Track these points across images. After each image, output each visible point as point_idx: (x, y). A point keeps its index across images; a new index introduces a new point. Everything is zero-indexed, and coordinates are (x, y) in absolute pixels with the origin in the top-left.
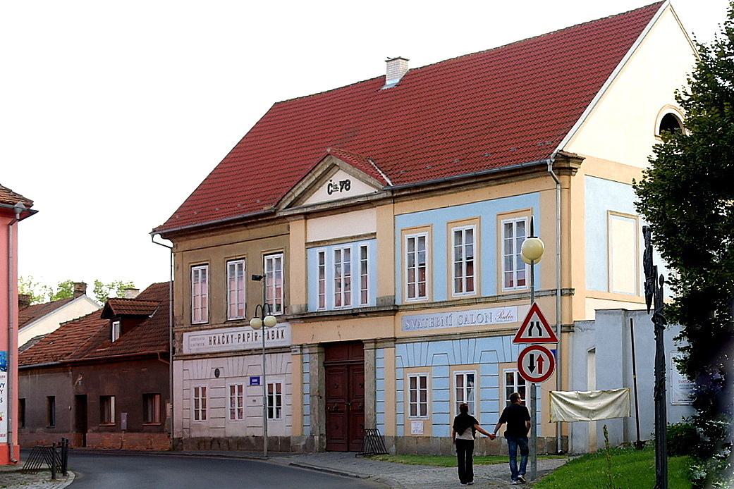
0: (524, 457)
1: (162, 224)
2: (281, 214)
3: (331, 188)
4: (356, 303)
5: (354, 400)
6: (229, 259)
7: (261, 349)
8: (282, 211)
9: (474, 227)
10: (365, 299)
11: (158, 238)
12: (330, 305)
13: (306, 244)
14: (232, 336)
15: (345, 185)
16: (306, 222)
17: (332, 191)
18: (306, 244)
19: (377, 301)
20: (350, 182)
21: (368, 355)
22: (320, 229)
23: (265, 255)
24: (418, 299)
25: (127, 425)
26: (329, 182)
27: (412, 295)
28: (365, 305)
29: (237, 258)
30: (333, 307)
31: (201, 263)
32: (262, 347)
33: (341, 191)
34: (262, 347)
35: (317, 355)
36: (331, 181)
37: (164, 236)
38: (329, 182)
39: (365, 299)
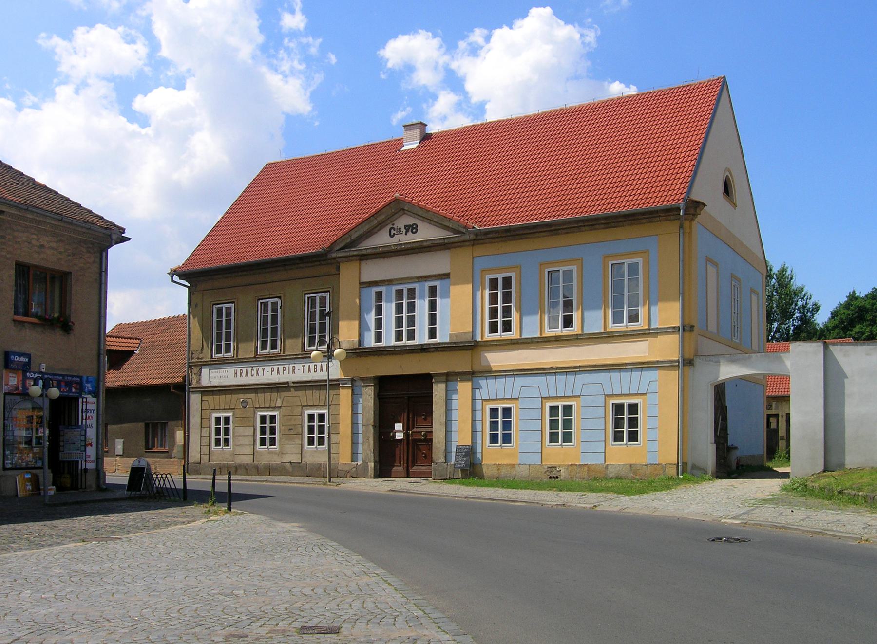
0: (459, 474)
1: (181, 265)
2: (334, 255)
3: (393, 232)
4: (422, 338)
5: (415, 430)
6: (261, 297)
7: (326, 381)
8: (334, 253)
9: (513, 275)
10: (432, 333)
11: (176, 278)
12: (389, 340)
13: (361, 283)
14: (263, 370)
15: (412, 229)
16: (360, 265)
17: (394, 234)
18: (361, 283)
19: (450, 338)
20: (417, 226)
21: (439, 390)
22: (373, 271)
23: (214, 304)
24: (500, 335)
25: (123, 450)
26: (390, 226)
27: (493, 329)
28: (433, 341)
29: (271, 296)
30: (393, 342)
31: (311, 292)
32: (327, 378)
33: (406, 234)
34: (327, 378)
35: (321, 391)
36: (393, 225)
37: (183, 276)
38: (390, 226)
39: (432, 333)
